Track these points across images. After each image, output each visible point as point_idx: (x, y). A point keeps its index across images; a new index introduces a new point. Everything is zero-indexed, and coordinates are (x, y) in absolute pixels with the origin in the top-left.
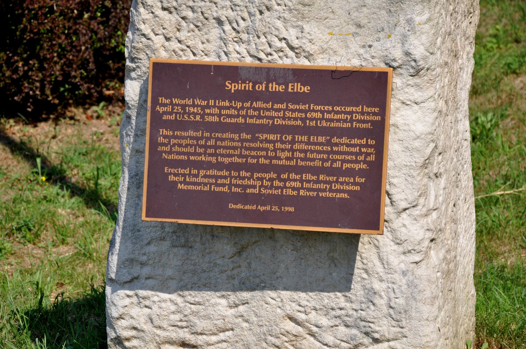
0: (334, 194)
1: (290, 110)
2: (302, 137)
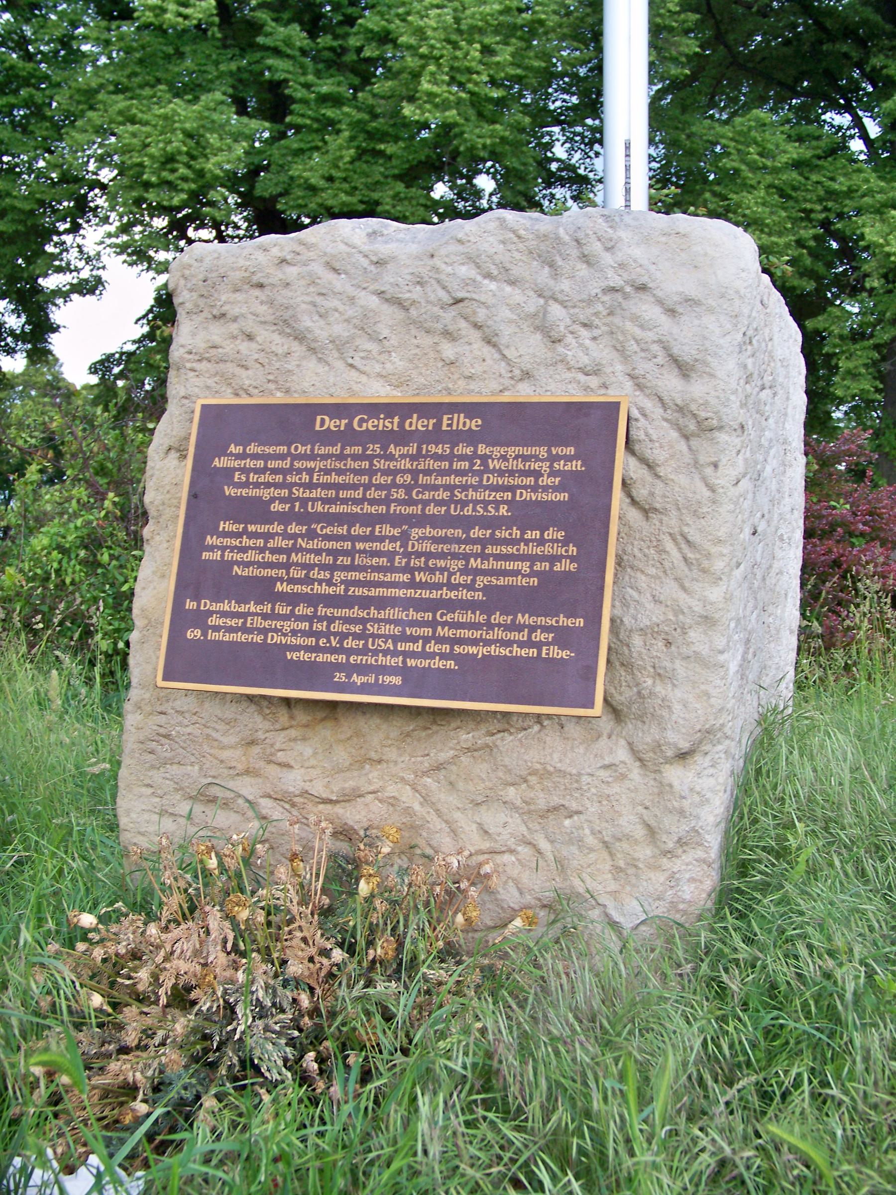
1: (457, 503)
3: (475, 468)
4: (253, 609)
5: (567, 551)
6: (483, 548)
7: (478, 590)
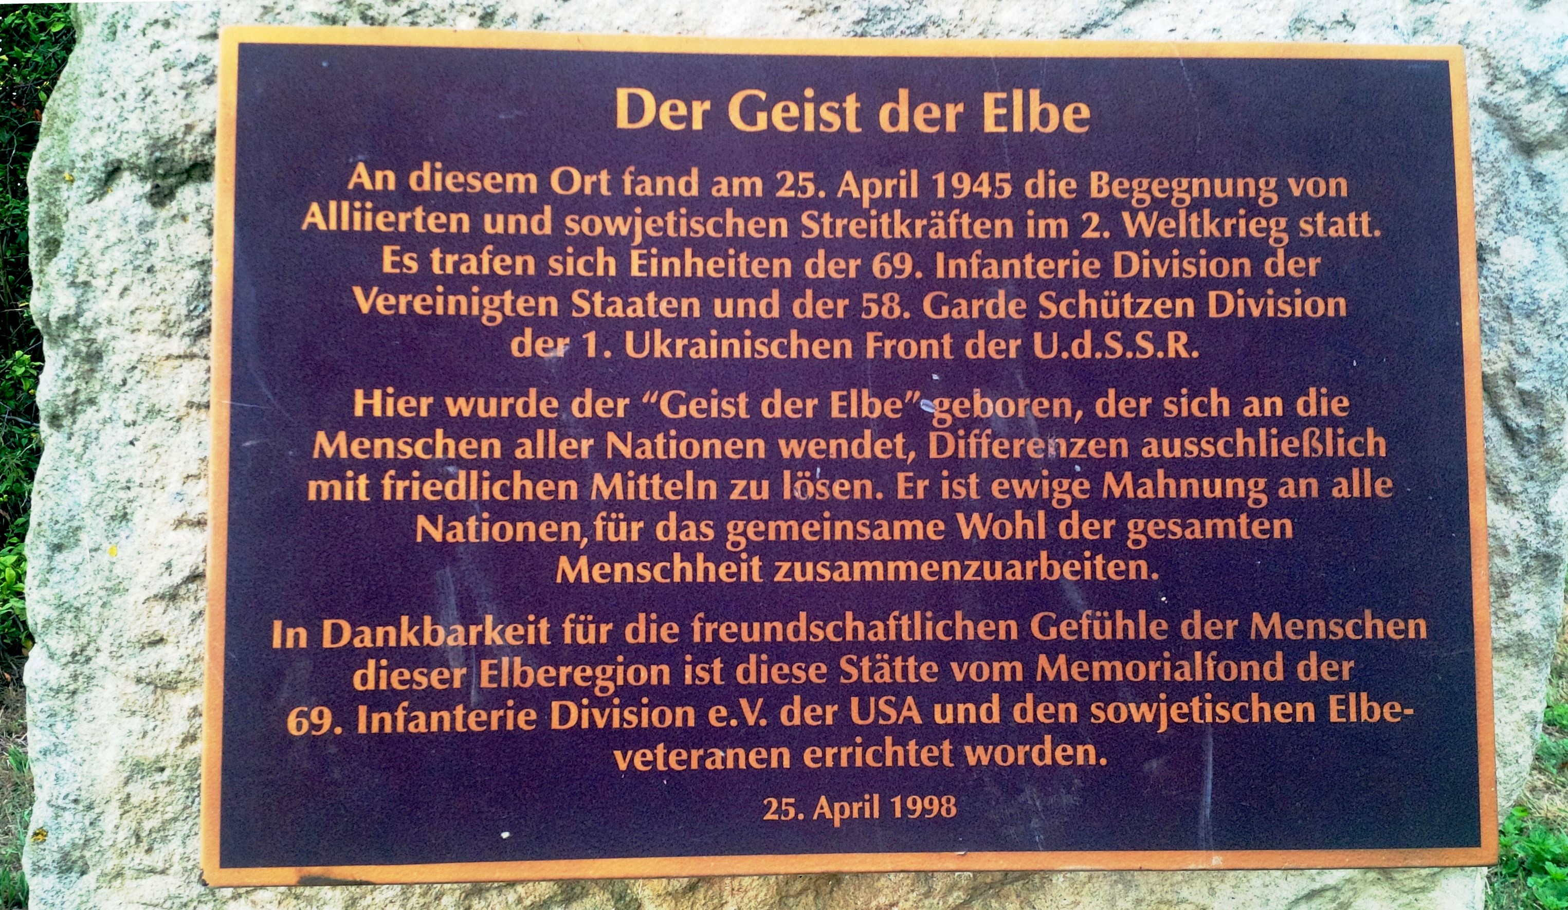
0: (696, 754)
2: (368, 395)
3: (1089, 234)
6: (1135, 448)
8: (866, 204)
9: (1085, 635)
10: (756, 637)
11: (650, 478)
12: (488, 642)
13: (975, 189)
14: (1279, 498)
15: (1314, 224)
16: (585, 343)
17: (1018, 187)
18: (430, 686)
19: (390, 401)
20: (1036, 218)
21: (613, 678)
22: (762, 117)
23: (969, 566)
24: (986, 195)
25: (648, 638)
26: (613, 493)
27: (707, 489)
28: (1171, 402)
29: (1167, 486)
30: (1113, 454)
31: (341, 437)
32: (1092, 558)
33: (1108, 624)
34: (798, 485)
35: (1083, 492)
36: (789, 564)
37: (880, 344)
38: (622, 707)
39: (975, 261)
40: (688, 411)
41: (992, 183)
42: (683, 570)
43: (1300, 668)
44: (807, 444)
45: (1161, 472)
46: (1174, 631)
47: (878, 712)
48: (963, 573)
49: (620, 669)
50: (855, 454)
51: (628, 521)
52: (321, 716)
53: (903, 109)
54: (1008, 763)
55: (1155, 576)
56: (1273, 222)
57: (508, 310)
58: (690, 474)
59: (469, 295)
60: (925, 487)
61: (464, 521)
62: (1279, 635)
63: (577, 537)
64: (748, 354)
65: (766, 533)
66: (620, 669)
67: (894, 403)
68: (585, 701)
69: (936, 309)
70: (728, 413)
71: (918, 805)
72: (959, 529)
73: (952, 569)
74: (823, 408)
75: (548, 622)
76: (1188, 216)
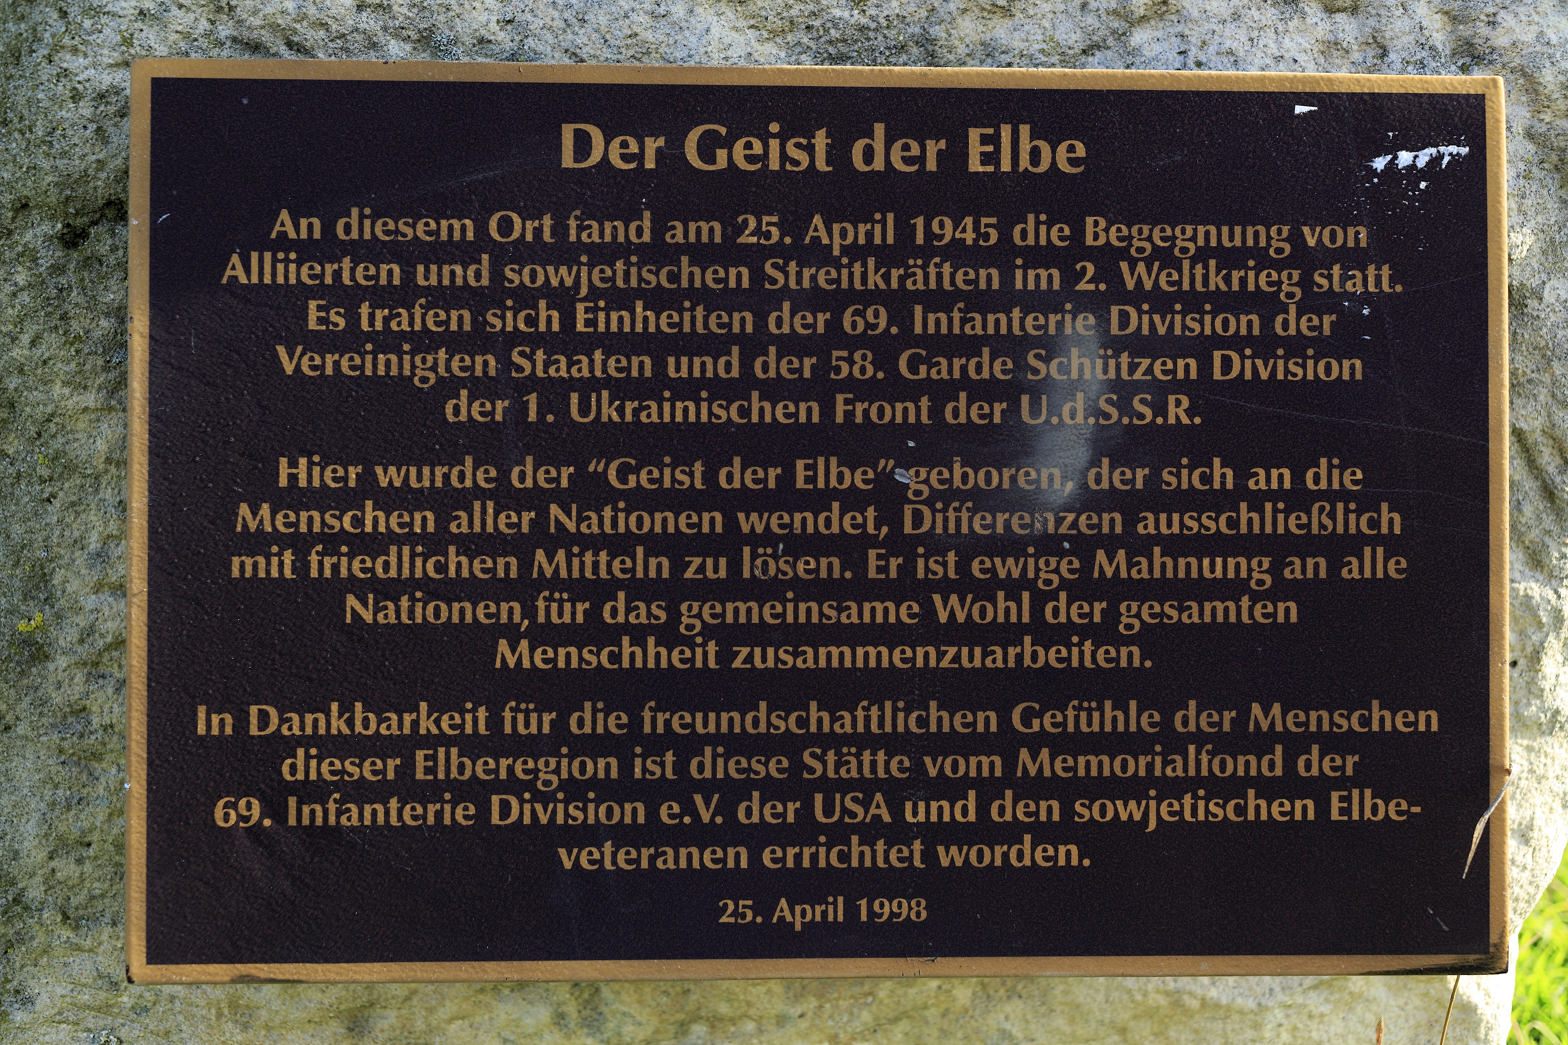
0: (645, 853)
2: (293, 464)
3: (1082, 286)
4: (426, 725)
5: (1374, 524)
6: (1130, 522)
7: (1128, 641)
8: (836, 252)
9: (1071, 728)
10: (712, 728)
11: (596, 554)
12: (423, 731)
13: (958, 235)
14: (1285, 579)
15: (1330, 277)
16: (525, 406)
17: (1005, 236)
18: (362, 777)
19: (316, 470)
20: (1025, 268)
21: (557, 771)
22: (722, 155)
23: (946, 652)
24: (969, 242)
25: (594, 728)
26: (557, 570)
27: (659, 566)
28: (1170, 473)
29: (1163, 565)
30: (1106, 530)
31: (265, 510)
32: (1080, 644)
33: (1096, 715)
34: (759, 562)
35: (1071, 571)
36: (749, 649)
37: (850, 407)
38: (567, 802)
39: (956, 315)
40: (638, 482)
41: (976, 229)
42: (632, 655)
43: (1301, 762)
44: (769, 518)
45: (1157, 550)
46: (1167, 723)
47: (845, 810)
48: (939, 661)
49: (565, 762)
50: (822, 528)
51: (573, 601)
52: (249, 806)
53: (879, 146)
54: (984, 865)
55: (1148, 664)
56: (1284, 274)
57: (441, 370)
58: (640, 550)
59: (400, 354)
60: (899, 565)
61: (396, 600)
62: (1279, 728)
63: (517, 618)
64: (704, 418)
65: (723, 615)
66: (565, 762)
67: (865, 473)
68: (527, 796)
69: (914, 370)
70: (681, 483)
71: (885, 908)
72: (935, 612)
73: (926, 655)
74: (787, 479)
75: (487, 710)
76: (1192, 268)
